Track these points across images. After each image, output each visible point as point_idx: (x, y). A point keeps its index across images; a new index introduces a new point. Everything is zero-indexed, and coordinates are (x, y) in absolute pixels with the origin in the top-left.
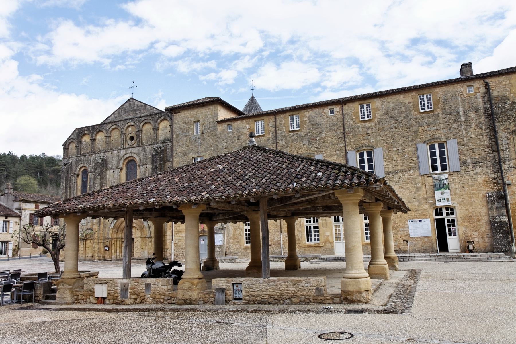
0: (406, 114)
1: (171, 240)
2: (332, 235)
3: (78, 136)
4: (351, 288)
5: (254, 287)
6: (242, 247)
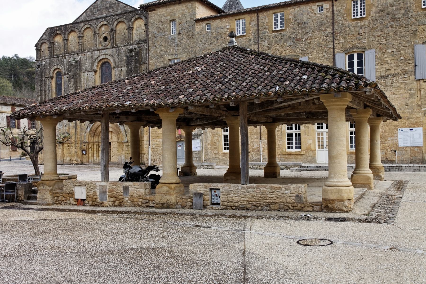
0: (406, 11)
2: (314, 142)
3: (50, 36)
5: (233, 192)
6: (220, 154)
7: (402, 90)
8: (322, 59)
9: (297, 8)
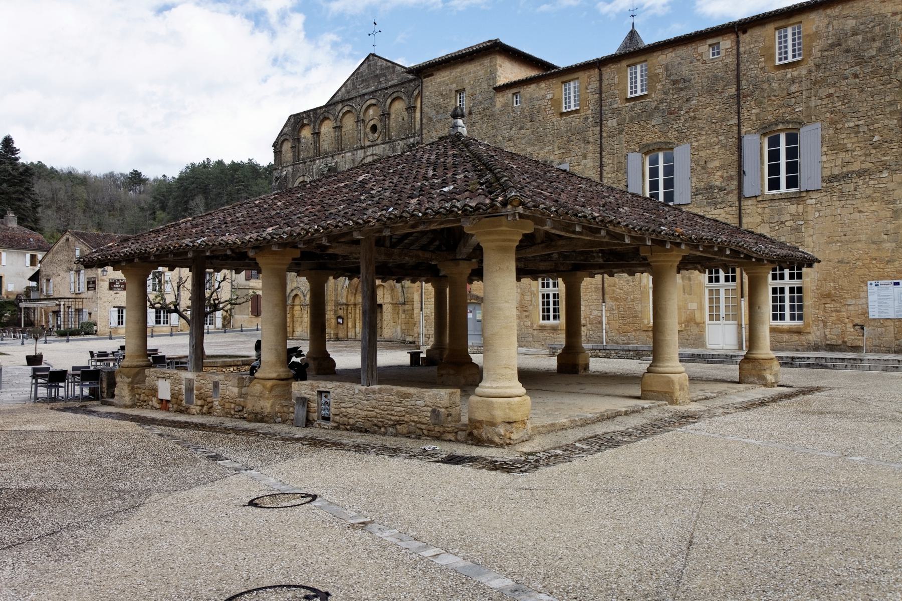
0: (885, 42)
1: (420, 309)
2: (701, 308)
3: (294, 129)
4: (480, 415)
5: (347, 399)
6: (535, 327)
7: (875, 203)
8: (717, 147)
9: (672, 52)
